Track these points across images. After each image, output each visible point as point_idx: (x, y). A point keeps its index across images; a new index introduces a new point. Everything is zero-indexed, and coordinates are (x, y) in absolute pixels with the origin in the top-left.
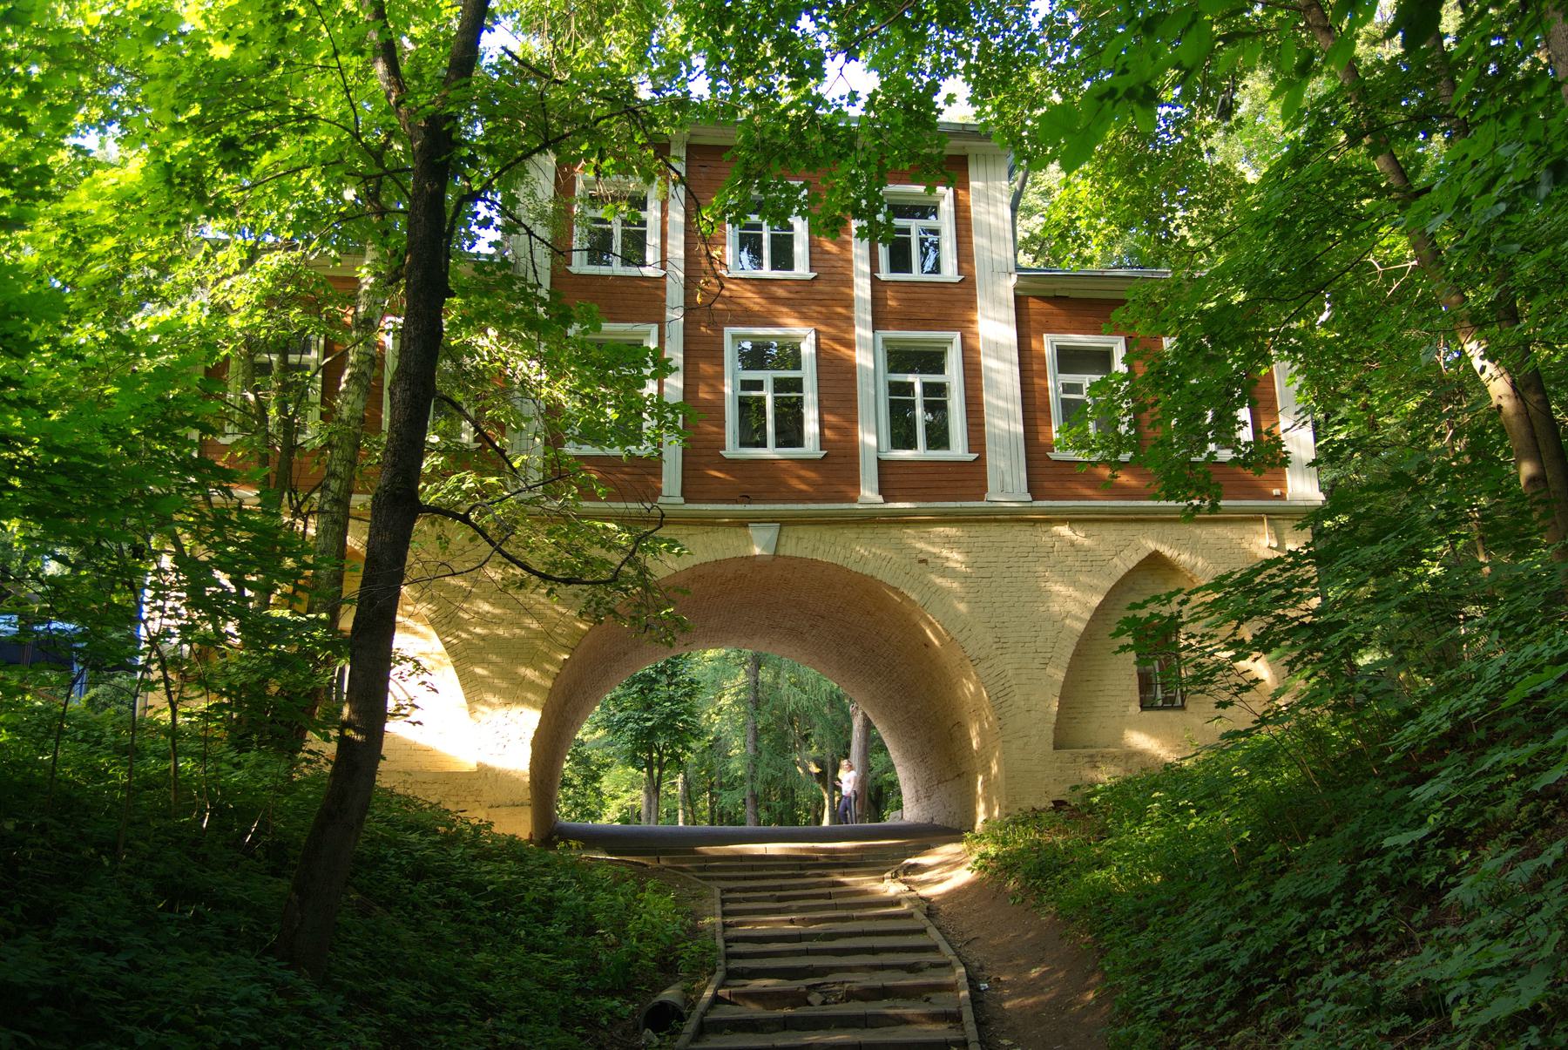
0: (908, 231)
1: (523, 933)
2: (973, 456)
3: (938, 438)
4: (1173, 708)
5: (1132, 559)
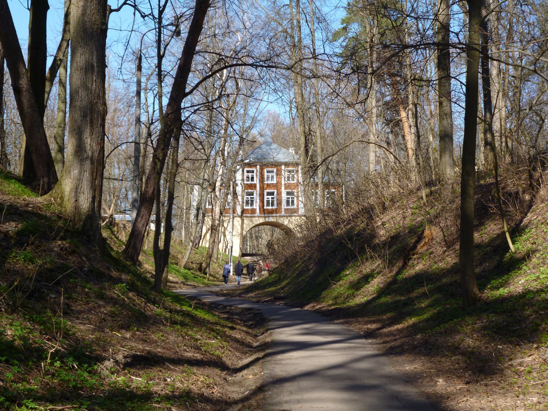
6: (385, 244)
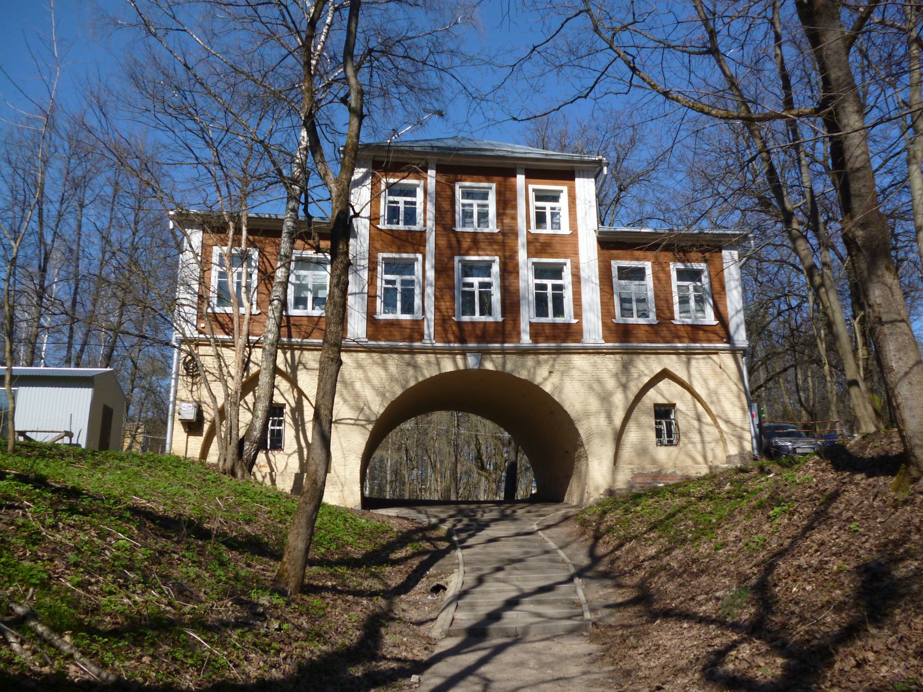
0: (545, 208)
1: (814, 480)
2: (576, 321)
3: (559, 311)
4: (671, 445)
5: (658, 370)
6: (378, 228)
